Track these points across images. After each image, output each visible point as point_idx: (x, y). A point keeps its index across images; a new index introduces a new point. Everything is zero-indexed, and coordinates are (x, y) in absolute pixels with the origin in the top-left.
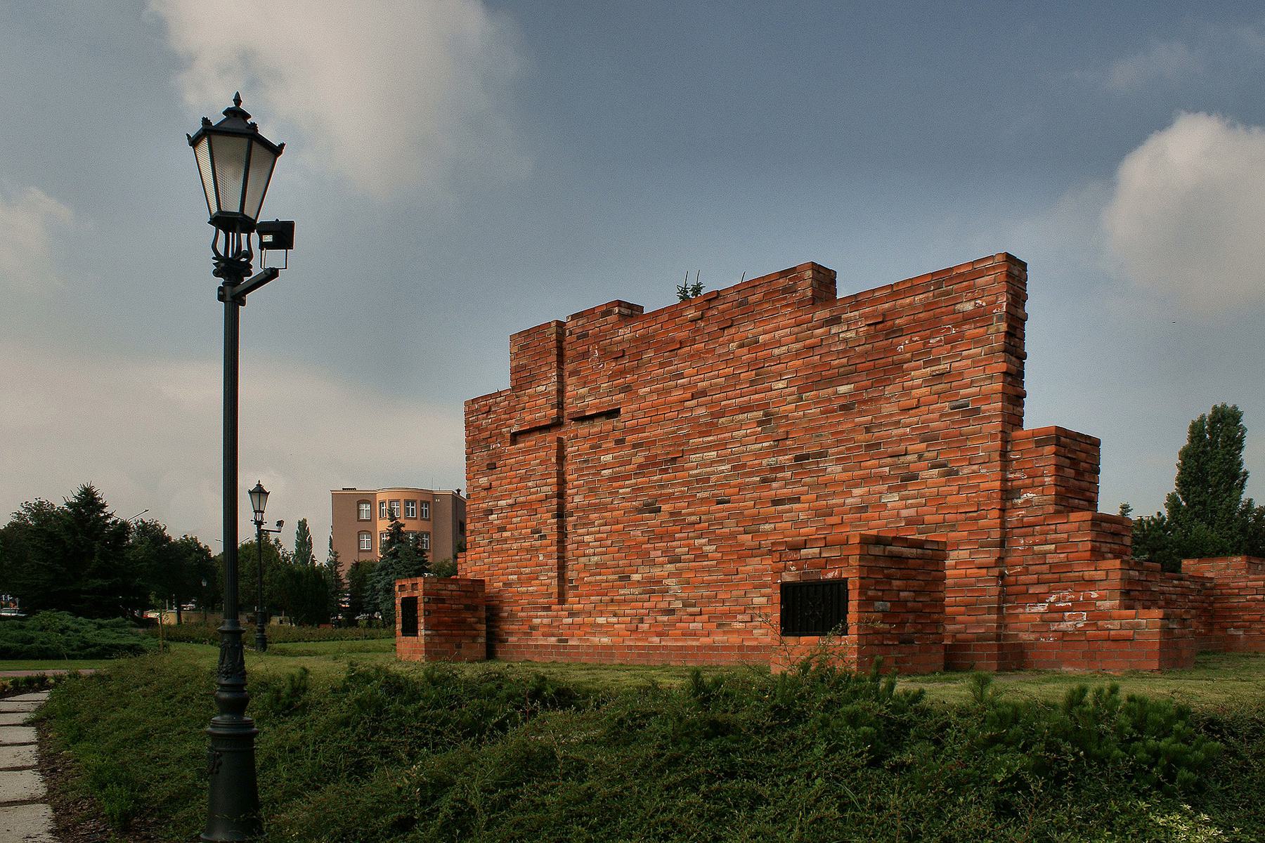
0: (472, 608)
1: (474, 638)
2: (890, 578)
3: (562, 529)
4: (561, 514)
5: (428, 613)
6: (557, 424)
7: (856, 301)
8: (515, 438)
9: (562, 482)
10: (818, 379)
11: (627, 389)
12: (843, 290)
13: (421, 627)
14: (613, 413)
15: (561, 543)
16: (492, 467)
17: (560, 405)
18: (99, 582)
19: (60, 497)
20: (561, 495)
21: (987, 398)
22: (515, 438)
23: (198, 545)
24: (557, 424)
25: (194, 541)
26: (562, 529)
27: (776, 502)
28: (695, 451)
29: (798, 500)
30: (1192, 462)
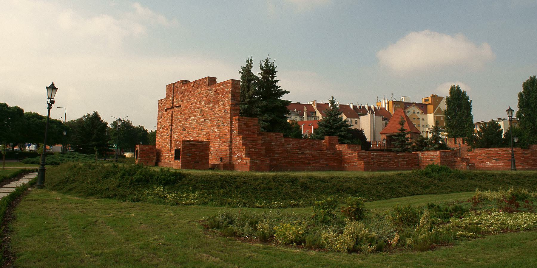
0: (152, 153)
1: (152, 160)
2: (192, 149)
3: (171, 134)
4: (171, 130)
5: (140, 154)
6: (172, 108)
7: (220, 84)
8: (166, 110)
9: (172, 122)
10: (208, 103)
11: (182, 101)
12: (218, 81)
13: (371, 173)
14: (180, 106)
15: (171, 137)
16: (162, 117)
17: (173, 103)
18: (95, 143)
19: (91, 113)
20: (172, 125)
21: (228, 110)
22: (166, 110)
23: (144, 129)
24: (172, 108)
25: (142, 127)
26: (171, 134)
27: (202, 130)
28: (192, 117)
29: (204, 129)
30: (140, 134)
